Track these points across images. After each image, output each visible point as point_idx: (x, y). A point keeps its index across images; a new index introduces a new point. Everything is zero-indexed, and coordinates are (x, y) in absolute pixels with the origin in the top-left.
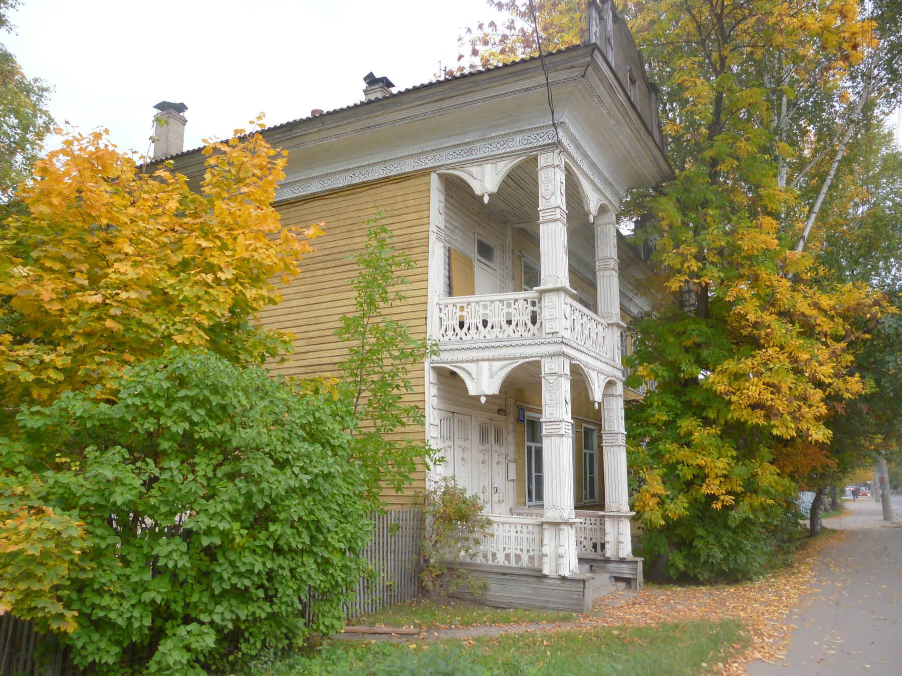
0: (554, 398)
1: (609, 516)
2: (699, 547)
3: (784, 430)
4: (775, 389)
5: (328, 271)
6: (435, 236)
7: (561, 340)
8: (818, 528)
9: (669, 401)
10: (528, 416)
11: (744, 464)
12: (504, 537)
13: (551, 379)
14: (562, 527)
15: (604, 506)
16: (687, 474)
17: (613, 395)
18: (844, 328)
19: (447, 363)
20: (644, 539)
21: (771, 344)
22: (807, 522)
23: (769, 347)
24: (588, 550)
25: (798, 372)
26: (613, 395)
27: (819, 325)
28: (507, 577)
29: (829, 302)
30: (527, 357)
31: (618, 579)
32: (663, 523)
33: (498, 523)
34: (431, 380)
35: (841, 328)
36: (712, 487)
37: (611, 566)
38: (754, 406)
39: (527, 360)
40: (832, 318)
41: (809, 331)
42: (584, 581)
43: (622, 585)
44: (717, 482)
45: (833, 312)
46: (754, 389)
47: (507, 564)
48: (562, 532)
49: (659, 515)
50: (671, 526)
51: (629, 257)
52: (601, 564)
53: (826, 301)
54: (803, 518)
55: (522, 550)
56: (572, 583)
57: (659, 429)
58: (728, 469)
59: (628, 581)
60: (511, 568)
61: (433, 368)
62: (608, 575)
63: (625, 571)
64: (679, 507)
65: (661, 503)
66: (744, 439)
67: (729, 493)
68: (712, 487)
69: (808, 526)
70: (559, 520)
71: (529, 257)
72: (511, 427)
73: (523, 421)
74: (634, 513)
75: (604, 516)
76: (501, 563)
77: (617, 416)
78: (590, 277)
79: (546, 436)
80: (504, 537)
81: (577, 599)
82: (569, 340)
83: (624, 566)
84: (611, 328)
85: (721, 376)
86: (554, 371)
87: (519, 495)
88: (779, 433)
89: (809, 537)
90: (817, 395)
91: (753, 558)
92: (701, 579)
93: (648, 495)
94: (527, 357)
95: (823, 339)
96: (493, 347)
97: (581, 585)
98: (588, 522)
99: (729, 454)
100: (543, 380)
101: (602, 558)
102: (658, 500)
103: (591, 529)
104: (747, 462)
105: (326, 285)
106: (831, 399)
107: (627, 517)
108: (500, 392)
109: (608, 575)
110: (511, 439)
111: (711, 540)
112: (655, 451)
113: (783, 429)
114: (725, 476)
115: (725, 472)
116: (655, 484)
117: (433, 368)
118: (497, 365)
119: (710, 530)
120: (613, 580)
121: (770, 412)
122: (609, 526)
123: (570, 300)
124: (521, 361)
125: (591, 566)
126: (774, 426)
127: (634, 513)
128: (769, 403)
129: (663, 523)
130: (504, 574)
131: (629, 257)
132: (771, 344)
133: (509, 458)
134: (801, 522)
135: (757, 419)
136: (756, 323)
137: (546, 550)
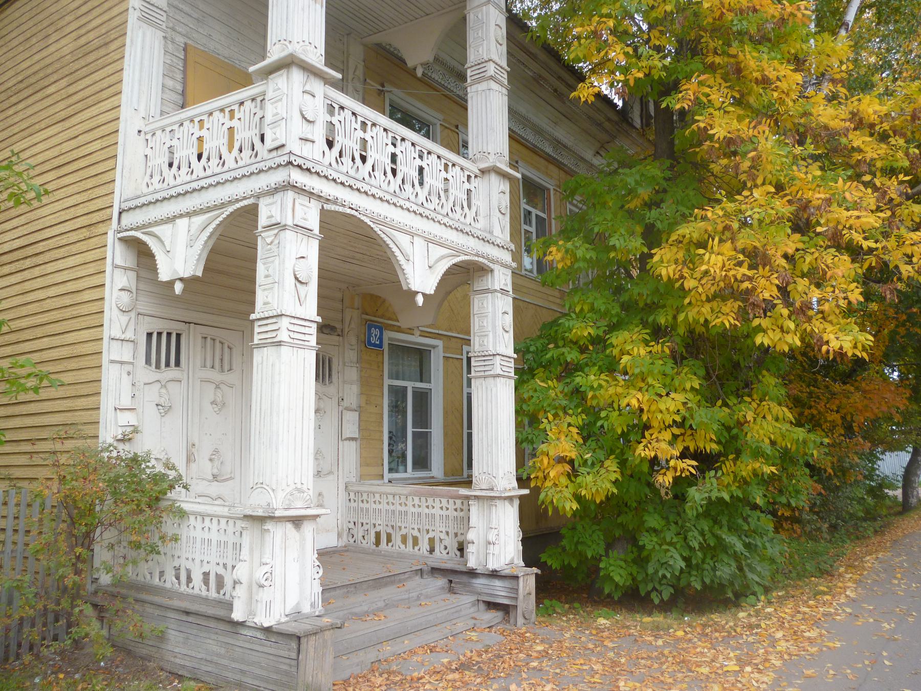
0: (271, 272)
1: (477, 498)
2: (649, 547)
3: (778, 335)
4: (756, 258)
5: (21, 106)
6: (137, 14)
7: (286, 158)
8: (914, 501)
9: (600, 305)
10: (390, 339)
11: (725, 404)
12: (203, 540)
13: (269, 236)
14: (269, 526)
15: (471, 482)
16: (616, 423)
17: (487, 291)
18: (907, 154)
19: (132, 229)
20: (540, 533)
21: (759, 181)
22: (899, 493)
23: (756, 186)
24: (452, 554)
25: (801, 225)
26: (487, 291)
27: (860, 150)
28: (190, 619)
29: (878, 108)
30: (237, 201)
31: (492, 606)
32: (575, 506)
33: (196, 514)
34: (119, 261)
35: (900, 154)
36: (659, 445)
37: (479, 582)
38: (719, 296)
39: (238, 205)
40: (884, 137)
41: (832, 154)
42: (299, 638)
43: (495, 616)
44: (667, 435)
45: (886, 126)
46: (716, 261)
47: (204, 593)
48: (268, 538)
49: (568, 493)
50: (594, 513)
51: (609, 120)
52: (465, 579)
53: (871, 107)
54: (893, 487)
55: (225, 566)
56: (280, 639)
57: (583, 350)
58: (683, 412)
59: (505, 609)
60: (206, 600)
61: (120, 239)
62: (473, 598)
63: (499, 591)
64: (601, 482)
65: (573, 474)
66: (723, 363)
67: (683, 456)
68: (659, 445)
69: (900, 498)
70: (260, 513)
71: (395, 90)
72: (351, 355)
73: (381, 346)
74: (526, 492)
75: (468, 498)
76: (196, 591)
77: (494, 327)
78: (461, 93)
79: (476, 378)
80: (203, 540)
81: (287, 673)
82: (318, 163)
83: (497, 583)
84: (486, 177)
85: (674, 249)
86: (273, 221)
87: (364, 462)
88: (766, 342)
89: (900, 514)
90: (842, 267)
91: (749, 566)
92: (657, 601)
93: (546, 461)
94: (237, 201)
95: (867, 178)
96: (194, 190)
97: (294, 645)
98: (451, 506)
99: (688, 387)
100: (259, 239)
101: (464, 569)
102: (568, 468)
103: (456, 518)
104: (732, 401)
105: (16, 129)
106: (878, 275)
107: (510, 499)
108: (206, 269)
109: (473, 598)
110: (352, 373)
111: (669, 536)
112: (571, 387)
113: (778, 335)
114: (680, 425)
115: (678, 419)
116: (562, 441)
117: (120, 239)
118: (199, 220)
119: (672, 518)
120: (482, 606)
121: (746, 300)
122: (475, 511)
123: (318, 87)
124: (231, 209)
125: (451, 582)
126: (759, 329)
127: (526, 492)
128: (746, 285)
129: (575, 506)
130: (187, 613)
131: (609, 120)
132: (759, 181)
133: (346, 403)
134: (891, 493)
135: (726, 318)
136: (729, 142)
137: (471, 536)
